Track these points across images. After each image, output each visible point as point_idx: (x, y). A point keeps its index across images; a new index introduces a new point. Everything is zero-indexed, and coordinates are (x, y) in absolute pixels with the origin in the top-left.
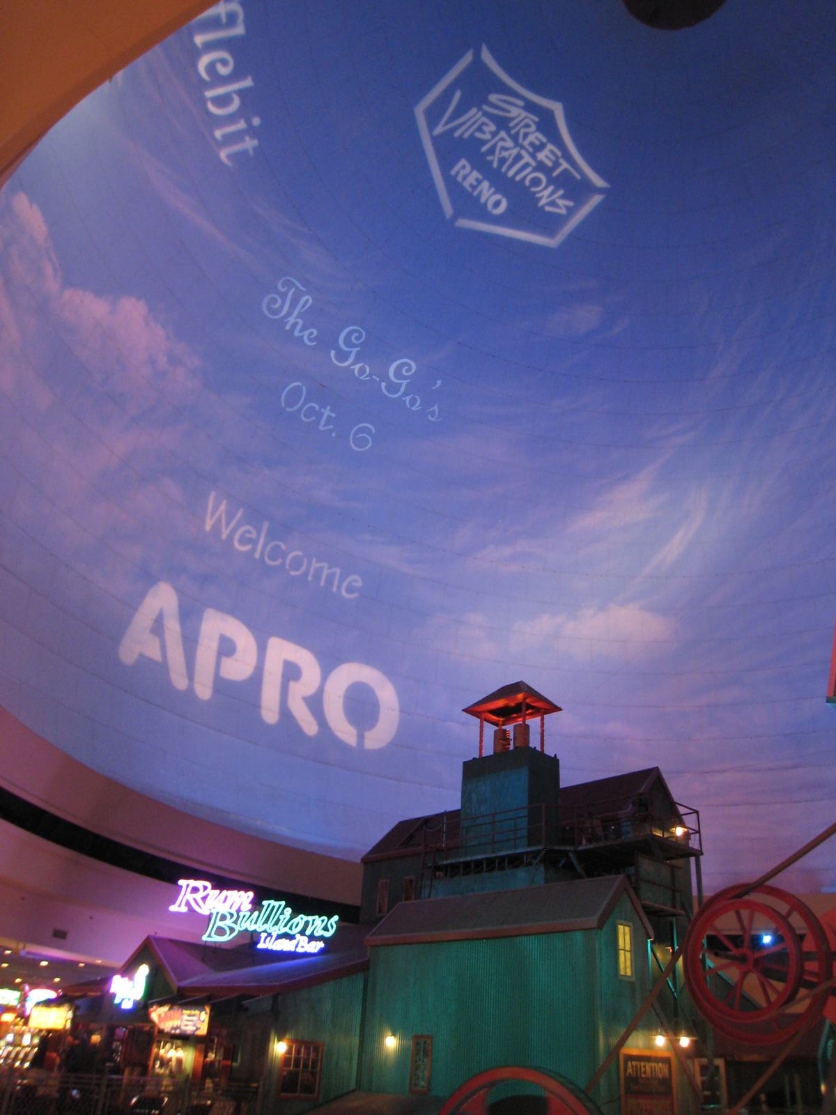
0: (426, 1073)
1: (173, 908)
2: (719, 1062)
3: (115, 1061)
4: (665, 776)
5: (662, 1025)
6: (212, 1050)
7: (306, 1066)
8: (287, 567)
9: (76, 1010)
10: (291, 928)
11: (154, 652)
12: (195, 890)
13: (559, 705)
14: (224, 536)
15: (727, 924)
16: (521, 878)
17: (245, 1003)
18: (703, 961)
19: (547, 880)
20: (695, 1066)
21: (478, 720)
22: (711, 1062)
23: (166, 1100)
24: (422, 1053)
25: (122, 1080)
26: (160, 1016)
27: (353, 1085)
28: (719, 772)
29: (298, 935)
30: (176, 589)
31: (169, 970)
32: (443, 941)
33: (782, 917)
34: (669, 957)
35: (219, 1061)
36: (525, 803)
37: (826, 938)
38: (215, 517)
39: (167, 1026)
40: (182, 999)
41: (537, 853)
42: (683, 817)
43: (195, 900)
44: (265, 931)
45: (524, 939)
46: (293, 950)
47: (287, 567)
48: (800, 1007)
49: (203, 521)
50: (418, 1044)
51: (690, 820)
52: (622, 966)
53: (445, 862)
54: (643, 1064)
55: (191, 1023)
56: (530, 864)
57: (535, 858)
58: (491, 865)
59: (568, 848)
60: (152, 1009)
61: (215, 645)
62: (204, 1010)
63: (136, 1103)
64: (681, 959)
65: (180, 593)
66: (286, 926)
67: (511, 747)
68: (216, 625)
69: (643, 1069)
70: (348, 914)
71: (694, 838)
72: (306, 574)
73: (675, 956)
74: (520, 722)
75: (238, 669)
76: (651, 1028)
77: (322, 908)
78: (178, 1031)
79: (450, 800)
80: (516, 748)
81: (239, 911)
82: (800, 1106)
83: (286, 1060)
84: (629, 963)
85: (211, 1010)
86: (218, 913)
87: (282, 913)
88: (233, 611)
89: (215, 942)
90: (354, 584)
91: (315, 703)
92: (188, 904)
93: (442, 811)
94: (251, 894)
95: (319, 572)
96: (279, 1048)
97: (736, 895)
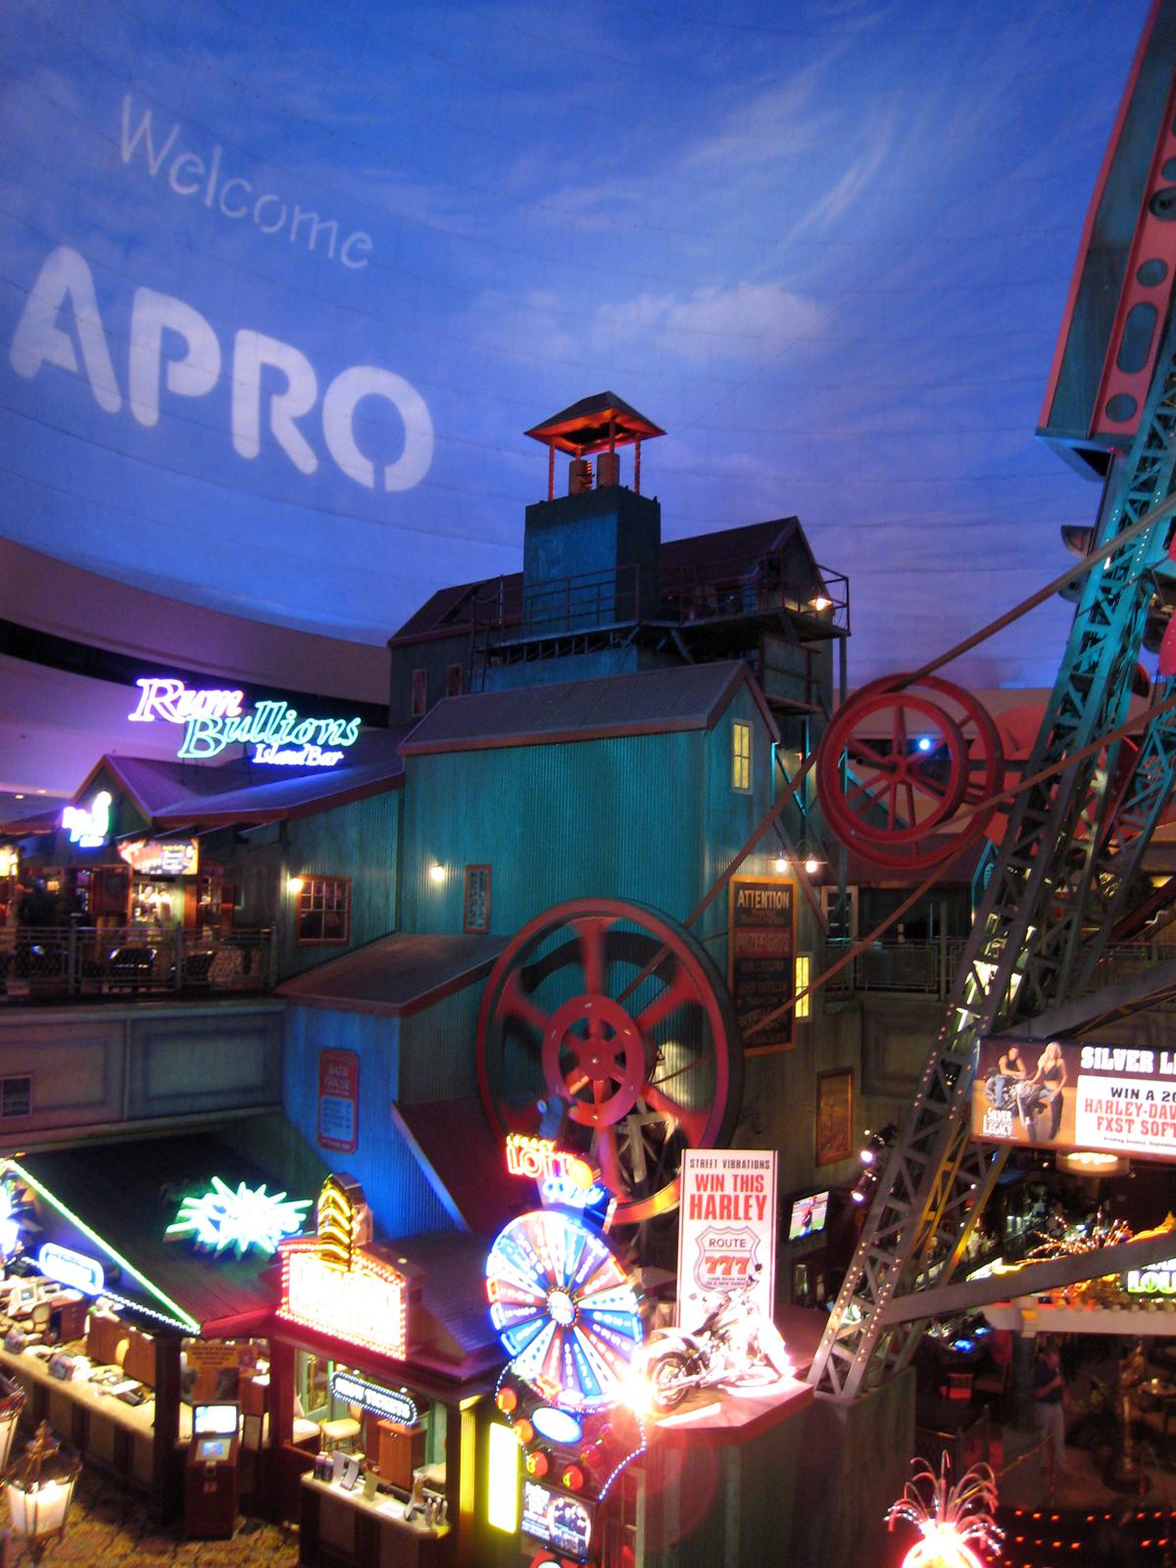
0: (484, 909)
1: (132, 717)
2: (853, 890)
3: (83, 911)
4: (805, 530)
5: (785, 848)
6: (206, 892)
7: (329, 907)
8: (257, 220)
9: (22, 853)
10: (297, 736)
11: (63, 356)
12: (162, 692)
13: (662, 427)
14: (153, 171)
15: (878, 724)
16: (605, 664)
17: (244, 833)
18: (842, 770)
19: (640, 666)
20: (822, 896)
21: (546, 449)
22: (842, 890)
23: (155, 952)
24: (478, 885)
25: (95, 932)
26: (133, 854)
27: (391, 926)
28: (880, 526)
29: (306, 744)
30: (88, 259)
31: (139, 797)
32: (503, 747)
33: (956, 725)
34: (798, 766)
35: (218, 905)
36: (612, 565)
37: (1001, 745)
38: (137, 137)
39: (144, 866)
40: (160, 832)
41: (627, 631)
42: (827, 585)
43: (162, 704)
44: (262, 742)
45: (610, 743)
46: (301, 763)
47: (257, 220)
48: (958, 826)
49: (118, 146)
50: (473, 875)
51: (837, 590)
52: (737, 777)
53: (503, 644)
54: (758, 893)
55: (176, 861)
56: (618, 646)
57: (625, 638)
58: (566, 647)
59: (669, 624)
60: (120, 847)
61: (156, 344)
62: (191, 844)
63: (116, 957)
64: (813, 768)
65: (96, 265)
66: (290, 733)
67: (594, 486)
68: (155, 313)
69: (758, 899)
70: (373, 715)
71: (841, 614)
72: (286, 229)
73: (806, 764)
74: (606, 450)
75: (195, 377)
76: (771, 851)
77: (339, 709)
78: (159, 872)
79: (509, 561)
80: (600, 487)
81: (224, 717)
82: (943, 936)
83: (304, 901)
84: (745, 773)
85: (200, 844)
86: (196, 721)
87: (284, 717)
88: (181, 290)
89: (196, 759)
90: (360, 246)
91: (311, 425)
92: (153, 710)
93: (497, 575)
94: (239, 695)
95: (305, 227)
96: (293, 886)
97: (892, 687)
